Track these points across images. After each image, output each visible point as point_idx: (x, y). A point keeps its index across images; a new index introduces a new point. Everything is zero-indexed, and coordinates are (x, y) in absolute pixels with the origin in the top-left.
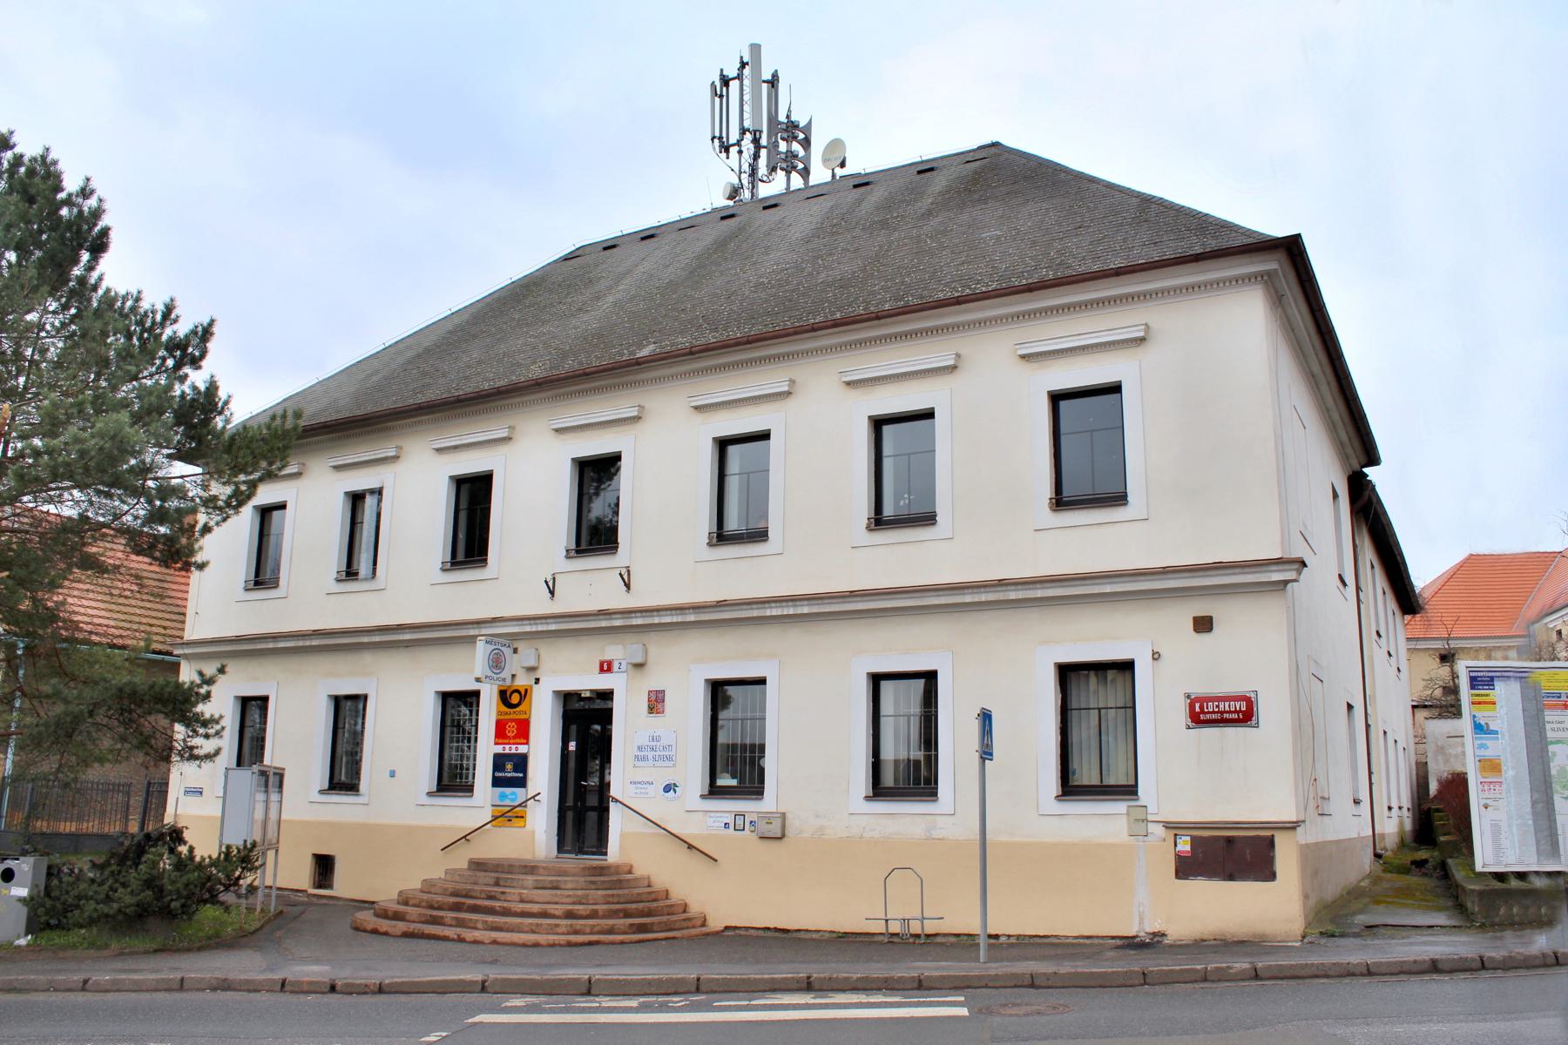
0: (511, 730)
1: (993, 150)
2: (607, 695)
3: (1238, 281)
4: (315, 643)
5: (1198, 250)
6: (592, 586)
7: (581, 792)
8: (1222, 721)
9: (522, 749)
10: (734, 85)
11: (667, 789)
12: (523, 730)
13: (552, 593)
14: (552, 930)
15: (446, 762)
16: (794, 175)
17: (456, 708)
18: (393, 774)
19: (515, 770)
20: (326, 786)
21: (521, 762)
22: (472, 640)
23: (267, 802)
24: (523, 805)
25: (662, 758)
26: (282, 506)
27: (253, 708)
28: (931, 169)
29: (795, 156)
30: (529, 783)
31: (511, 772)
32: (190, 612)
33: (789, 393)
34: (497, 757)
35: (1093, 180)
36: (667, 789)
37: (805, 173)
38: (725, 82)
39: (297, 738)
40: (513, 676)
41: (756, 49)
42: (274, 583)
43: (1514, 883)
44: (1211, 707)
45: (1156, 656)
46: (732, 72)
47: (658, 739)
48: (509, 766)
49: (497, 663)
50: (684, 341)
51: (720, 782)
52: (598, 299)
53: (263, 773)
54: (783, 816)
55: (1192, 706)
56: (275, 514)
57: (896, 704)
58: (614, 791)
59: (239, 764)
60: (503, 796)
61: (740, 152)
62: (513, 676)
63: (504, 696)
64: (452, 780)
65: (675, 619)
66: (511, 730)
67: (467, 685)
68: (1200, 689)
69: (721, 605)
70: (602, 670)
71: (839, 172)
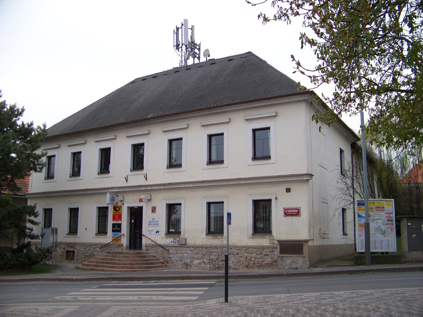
0: (117, 217)
1: (249, 54)
2: (141, 208)
3: (299, 101)
4: (65, 194)
5: (289, 93)
6: (137, 179)
7: (135, 233)
8: (292, 215)
9: (120, 222)
10: (180, 30)
11: (157, 232)
12: (120, 217)
13: (127, 180)
14: (126, 267)
15: (212, 215)
16: (196, 59)
17: (102, 212)
18: (86, 229)
19: (118, 228)
20: (68, 232)
21: (119, 226)
22: (106, 193)
23: (53, 237)
24: (120, 237)
25: (155, 224)
26: (54, 156)
27: (48, 212)
28: (232, 60)
29: (196, 53)
30: (122, 231)
31: (117, 228)
32: (30, 185)
33: (187, 128)
34: (113, 224)
35: (78, 216)
36: (157, 232)
37: (199, 58)
38: (178, 29)
39: (61, 220)
40: (117, 203)
41: (186, 21)
42: (53, 177)
43: (385, 255)
44: (289, 211)
45: (276, 198)
46: (180, 26)
47: (154, 219)
48: (116, 227)
49: (112, 199)
50: (160, 113)
51: (171, 230)
52: (139, 97)
53: (52, 230)
54: (186, 239)
55: (285, 211)
56: (52, 158)
57: (215, 210)
58: (143, 233)
59: (45, 227)
60: (115, 235)
61: (182, 50)
62: (117, 203)
63: (115, 208)
64: (102, 230)
65: (158, 188)
66: (117, 217)
67: (105, 205)
68: (287, 206)
69: (170, 184)
70: (140, 201)
71: (208, 58)
